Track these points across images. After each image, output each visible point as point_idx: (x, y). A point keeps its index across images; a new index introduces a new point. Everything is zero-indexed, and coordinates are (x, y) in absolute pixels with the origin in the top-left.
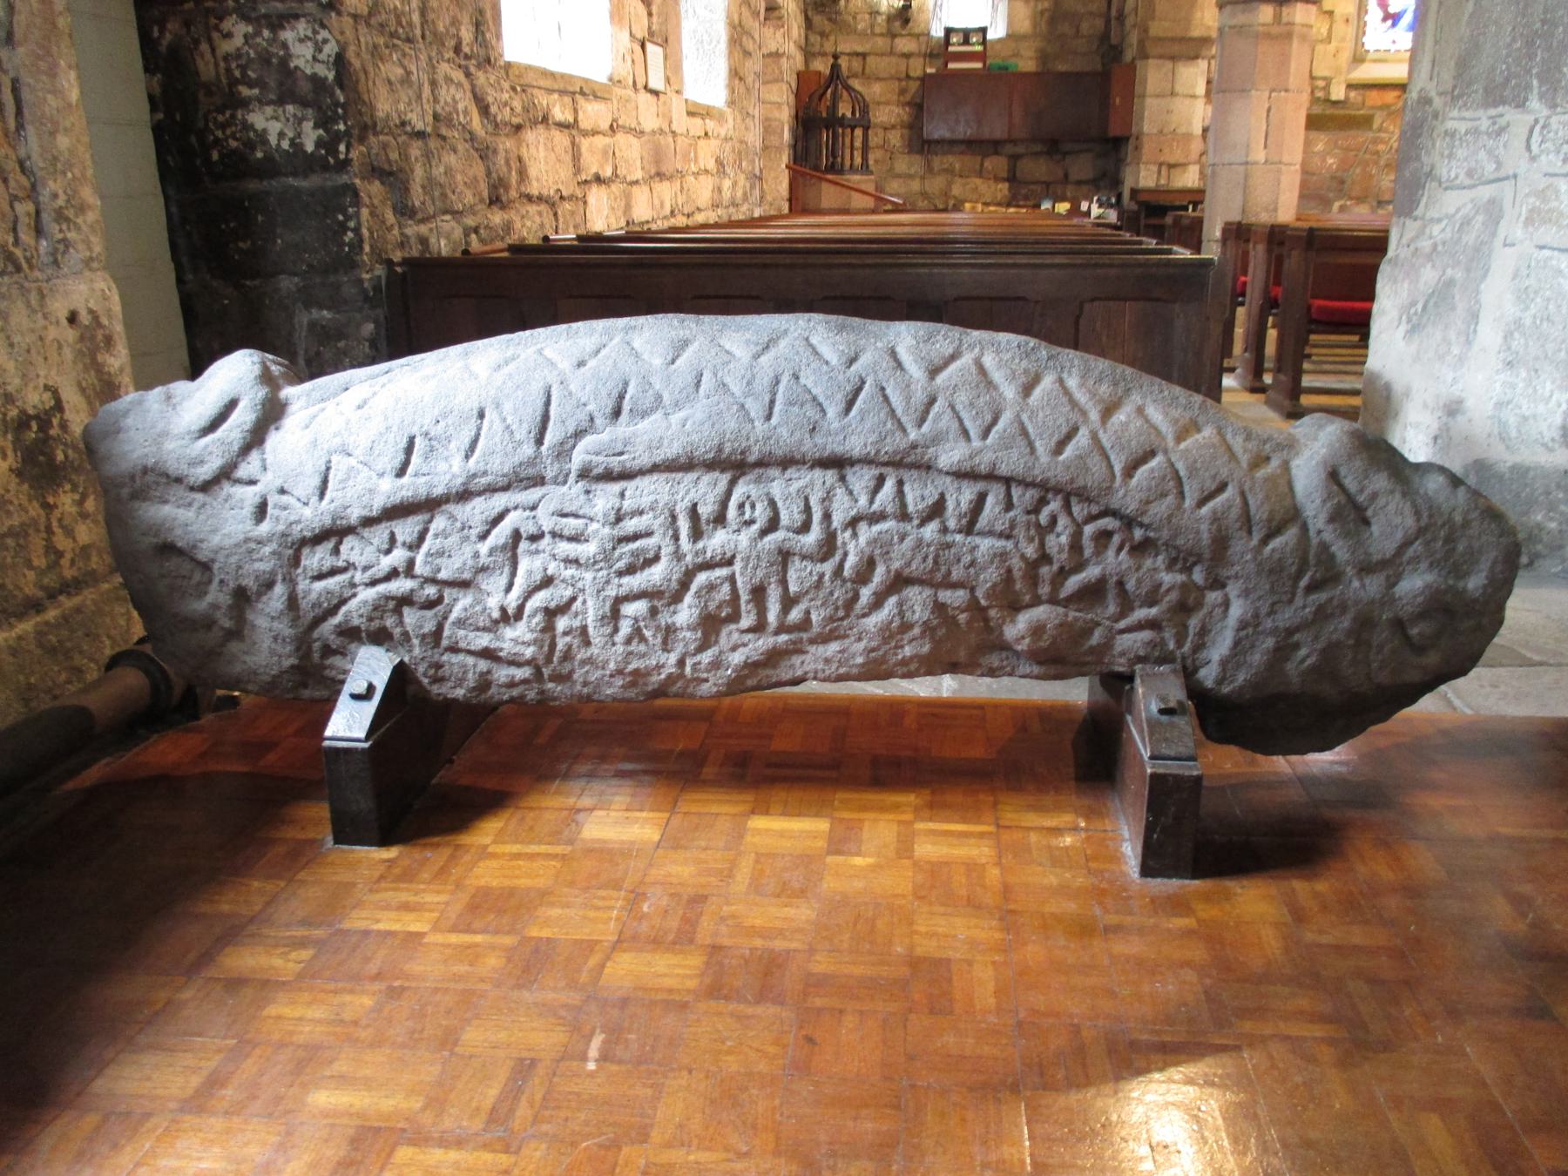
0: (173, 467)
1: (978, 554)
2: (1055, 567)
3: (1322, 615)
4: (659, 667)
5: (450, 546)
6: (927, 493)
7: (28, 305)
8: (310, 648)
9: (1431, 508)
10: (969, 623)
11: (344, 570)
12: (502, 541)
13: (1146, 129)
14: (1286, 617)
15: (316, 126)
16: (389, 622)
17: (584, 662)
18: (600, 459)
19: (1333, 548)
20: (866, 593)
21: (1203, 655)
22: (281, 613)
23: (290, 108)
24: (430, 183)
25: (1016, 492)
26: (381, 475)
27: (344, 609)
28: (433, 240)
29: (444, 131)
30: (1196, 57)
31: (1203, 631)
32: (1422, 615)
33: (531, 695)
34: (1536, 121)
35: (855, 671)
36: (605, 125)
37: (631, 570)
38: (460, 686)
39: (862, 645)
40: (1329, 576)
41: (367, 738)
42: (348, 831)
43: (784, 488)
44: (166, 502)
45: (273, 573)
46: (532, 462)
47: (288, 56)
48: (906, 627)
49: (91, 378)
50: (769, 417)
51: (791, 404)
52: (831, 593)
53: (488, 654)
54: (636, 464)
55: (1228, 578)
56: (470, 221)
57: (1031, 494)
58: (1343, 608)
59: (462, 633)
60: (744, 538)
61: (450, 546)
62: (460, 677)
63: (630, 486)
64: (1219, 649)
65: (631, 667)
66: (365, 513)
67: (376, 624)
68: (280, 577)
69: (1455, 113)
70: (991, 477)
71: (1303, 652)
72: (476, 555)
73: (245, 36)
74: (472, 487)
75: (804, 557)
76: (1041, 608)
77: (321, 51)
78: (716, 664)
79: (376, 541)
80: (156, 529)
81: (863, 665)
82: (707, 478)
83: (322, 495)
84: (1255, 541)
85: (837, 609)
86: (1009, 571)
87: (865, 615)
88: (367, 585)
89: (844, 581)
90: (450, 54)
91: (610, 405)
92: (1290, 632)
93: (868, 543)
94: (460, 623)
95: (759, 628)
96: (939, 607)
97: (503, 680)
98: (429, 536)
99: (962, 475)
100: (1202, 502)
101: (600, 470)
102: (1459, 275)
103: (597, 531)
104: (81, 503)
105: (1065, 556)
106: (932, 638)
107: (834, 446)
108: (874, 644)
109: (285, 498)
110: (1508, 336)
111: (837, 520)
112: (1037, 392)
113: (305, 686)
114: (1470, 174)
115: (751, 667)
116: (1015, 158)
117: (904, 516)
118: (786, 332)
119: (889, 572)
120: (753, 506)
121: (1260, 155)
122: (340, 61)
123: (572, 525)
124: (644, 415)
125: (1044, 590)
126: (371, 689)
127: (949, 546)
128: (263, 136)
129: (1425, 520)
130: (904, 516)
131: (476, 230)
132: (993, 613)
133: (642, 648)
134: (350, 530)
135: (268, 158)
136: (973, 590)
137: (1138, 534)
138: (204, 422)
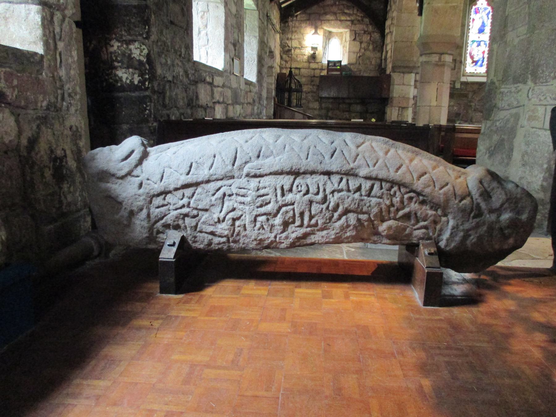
0: (113, 171)
1: (372, 203)
2: (395, 208)
3: (477, 226)
4: (268, 238)
5: (202, 197)
6: (356, 183)
7: (59, 122)
8: (153, 231)
9: (510, 193)
10: (368, 225)
11: (167, 205)
12: (219, 196)
13: (394, 95)
14: (467, 226)
15: (139, 76)
16: (181, 222)
17: (244, 236)
18: (253, 170)
19: (481, 204)
20: (336, 215)
21: (441, 237)
22: (145, 219)
23: (131, 70)
24: (171, 98)
25: (384, 184)
26: (181, 174)
27: (165, 218)
28: (171, 116)
29: (175, 81)
30: (411, 73)
31: (441, 230)
32: (508, 227)
33: (225, 247)
34: (530, 88)
35: (331, 240)
36: (221, 84)
37: (261, 206)
38: (202, 244)
39: (334, 232)
40: (479, 214)
41: (174, 258)
42: (164, 290)
43: (311, 181)
44: (108, 182)
45: (143, 206)
46: (231, 171)
47: (131, 53)
48: (348, 226)
49: (74, 148)
50: (307, 159)
51: (314, 155)
52: (325, 215)
53: (212, 233)
54: (265, 173)
55: (449, 213)
56: (181, 111)
57: (388, 185)
58: (484, 223)
59: (204, 226)
60: (298, 196)
61: (202, 197)
62: (201, 242)
63: (262, 179)
64: (446, 235)
65: (259, 238)
66: (176, 186)
67: (176, 223)
68: (145, 207)
69: (503, 86)
70: (376, 179)
71: (472, 237)
72: (211, 201)
73: (118, 47)
74: (211, 179)
75: (317, 203)
76: (391, 221)
77: (142, 52)
78: (287, 238)
79: (178, 196)
80: (107, 190)
81: (334, 238)
82: (287, 177)
83: (161, 180)
84: (457, 202)
85: (326, 220)
86: (381, 209)
87: (335, 222)
88: (174, 210)
89: (329, 211)
90: (178, 57)
91: (257, 154)
92: (468, 230)
93: (337, 199)
94: (204, 223)
95: (301, 226)
96: (359, 220)
97: (217, 242)
98: (195, 195)
99: (367, 178)
100: (441, 188)
101: (253, 174)
102: (506, 137)
103: (251, 194)
104: (69, 188)
105: (398, 204)
106: (356, 229)
107: (328, 168)
108: (338, 231)
109: (149, 181)
110: (523, 156)
111: (328, 191)
112: (389, 154)
113: (150, 244)
114: (509, 105)
115: (298, 239)
116: (350, 104)
117: (349, 190)
118: (311, 134)
119: (343, 208)
120: (301, 186)
121: (434, 103)
122: (148, 56)
123: (243, 191)
124: (267, 157)
125: (392, 215)
126: (174, 243)
127: (362, 200)
128: (121, 79)
129: (509, 196)
130: (349, 190)
131: (183, 114)
132: (375, 222)
133: (263, 231)
134: (170, 192)
135: (122, 86)
136: (369, 215)
137: (421, 198)
138: (123, 157)
